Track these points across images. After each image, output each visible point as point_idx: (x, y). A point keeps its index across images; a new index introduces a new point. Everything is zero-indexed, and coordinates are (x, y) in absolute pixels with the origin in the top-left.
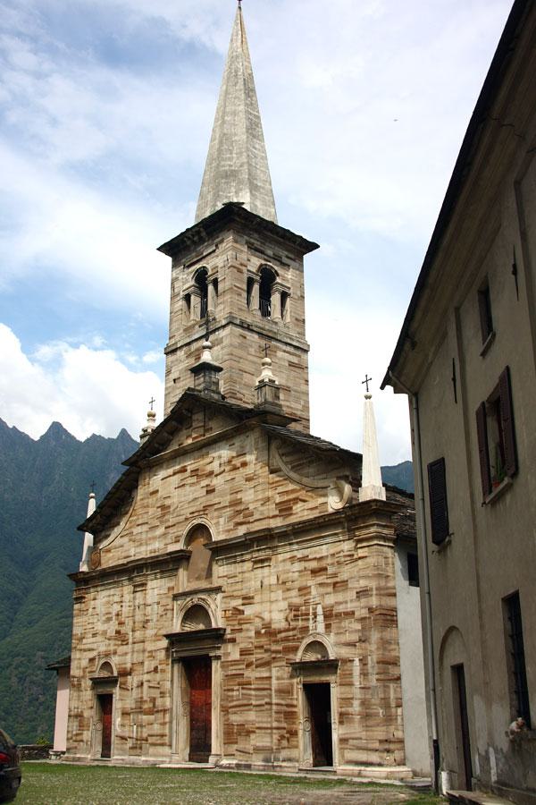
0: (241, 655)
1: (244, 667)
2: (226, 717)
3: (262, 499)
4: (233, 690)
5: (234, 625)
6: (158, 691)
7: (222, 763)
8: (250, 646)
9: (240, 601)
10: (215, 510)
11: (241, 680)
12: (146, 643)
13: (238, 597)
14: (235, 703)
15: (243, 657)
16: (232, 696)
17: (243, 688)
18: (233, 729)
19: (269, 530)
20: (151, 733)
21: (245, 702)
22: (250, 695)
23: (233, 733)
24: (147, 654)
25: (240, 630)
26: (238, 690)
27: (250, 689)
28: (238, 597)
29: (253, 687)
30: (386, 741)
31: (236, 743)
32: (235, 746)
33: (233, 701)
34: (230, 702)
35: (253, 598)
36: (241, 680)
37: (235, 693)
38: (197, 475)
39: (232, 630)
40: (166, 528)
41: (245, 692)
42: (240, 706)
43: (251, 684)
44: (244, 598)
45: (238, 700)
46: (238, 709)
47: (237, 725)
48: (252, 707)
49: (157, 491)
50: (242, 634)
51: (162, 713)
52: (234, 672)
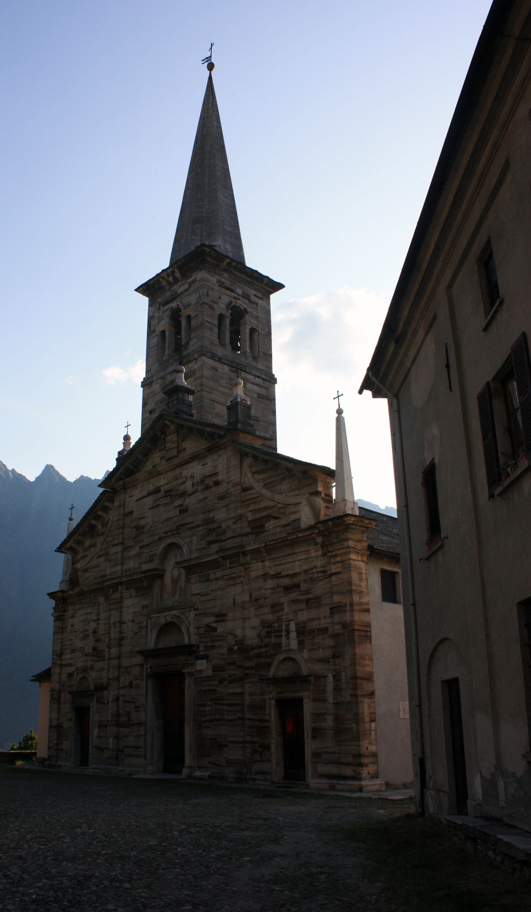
0: (213, 671)
1: (216, 683)
4: (205, 705)
9: (213, 619)
17: (216, 704)
27: (223, 704)
29: (225, 702)
37: (207, 708)
38: (171, 496)
39: (205, 647)
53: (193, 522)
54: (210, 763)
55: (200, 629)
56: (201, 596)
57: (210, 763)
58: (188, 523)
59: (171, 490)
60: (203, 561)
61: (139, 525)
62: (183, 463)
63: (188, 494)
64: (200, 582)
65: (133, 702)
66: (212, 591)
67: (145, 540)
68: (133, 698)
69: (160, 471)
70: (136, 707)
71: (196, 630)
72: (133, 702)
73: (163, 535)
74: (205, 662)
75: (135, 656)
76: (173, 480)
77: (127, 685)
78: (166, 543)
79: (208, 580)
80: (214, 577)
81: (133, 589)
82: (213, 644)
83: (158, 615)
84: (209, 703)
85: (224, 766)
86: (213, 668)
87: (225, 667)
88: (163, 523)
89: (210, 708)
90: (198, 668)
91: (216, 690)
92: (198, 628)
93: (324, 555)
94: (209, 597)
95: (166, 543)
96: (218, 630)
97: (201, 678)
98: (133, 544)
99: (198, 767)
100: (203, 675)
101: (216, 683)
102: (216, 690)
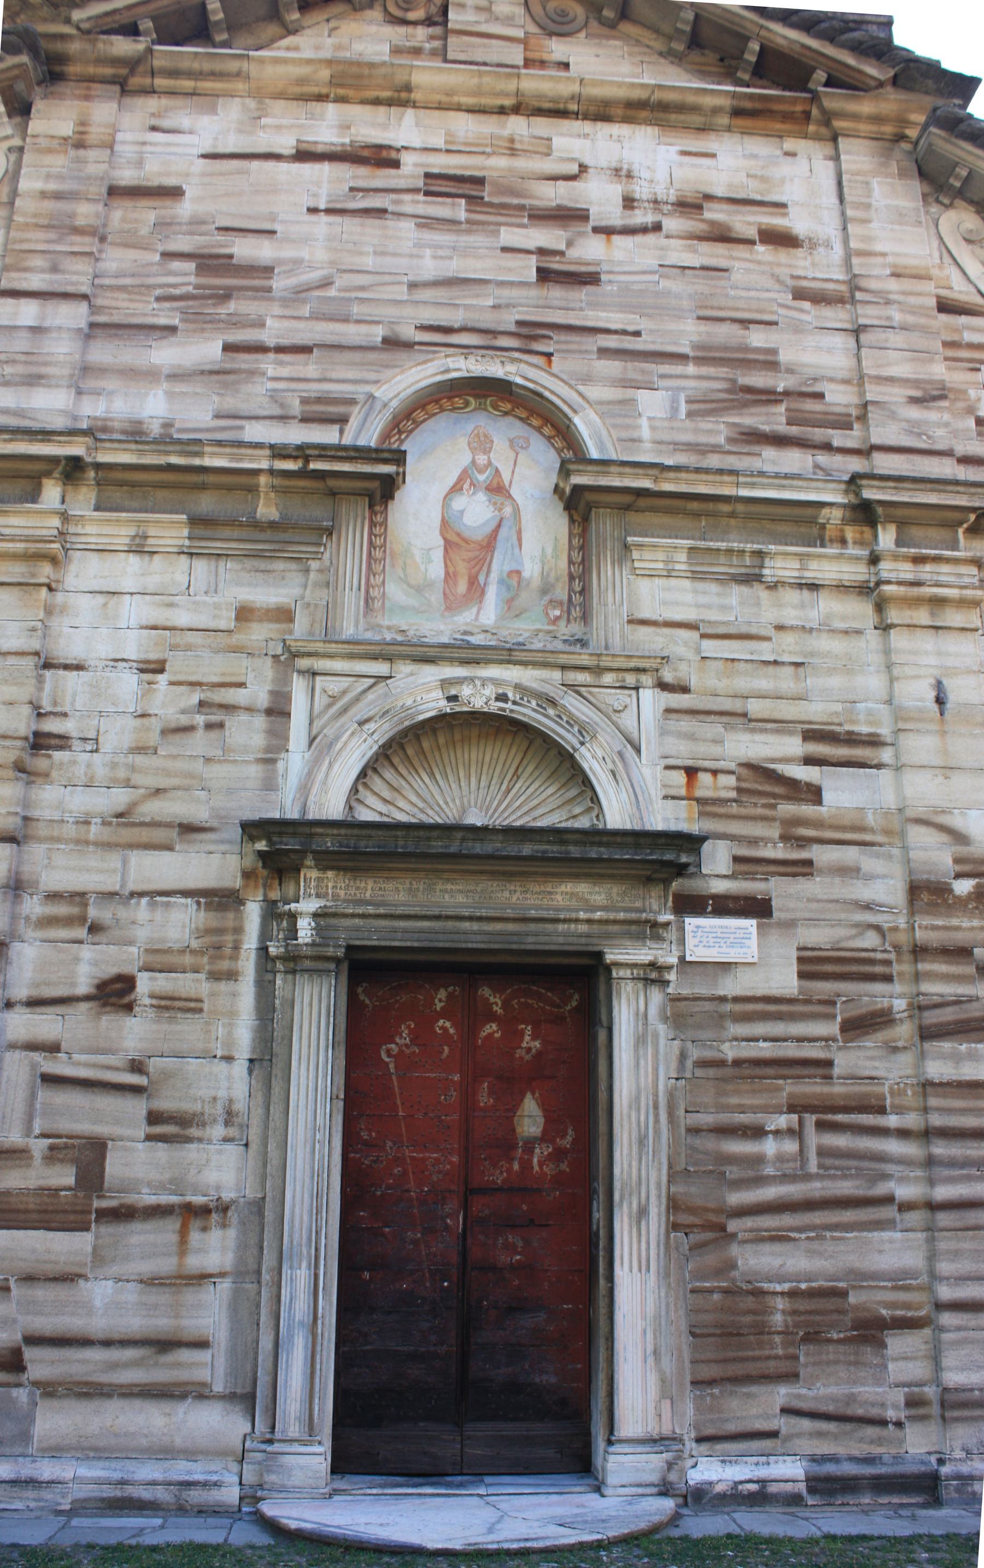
0: (802, 975)
1: (832, 1029)
2: (711, 1259)
3: (916, 383)
4: (758, 1132)
5: (754, 842)
6: (137, 1108)
7: (696, 1476)
8: (870, 940)
9: (794, 746)
10: (604, 352)
11: (812, 1088)
12: (37, 851)
13: (780, 725)
14: (769, 1193)
15: (825, 988)
16: (759, 1160)
17: (822, 1126)
18: (768, 1311)
19: (783, 122)
20: (45, 1324)
21: (846, 1188)
22: (881, 1158)
23: (761, 1330)
24: (33, 906)
25: (805, 868)
26: (796, 1133)
27: (883, 1132)
28: (780, 725)
29: (892, 1121)
30: (133, 486)
31: (791, 1377)
32: (782, 1394)
33: (760, 1181)
34: (738, 1184)
35: (874, 742)
36: (812, 1088)
37: (769, 1147)
38: (471, 199)
39: (737, 859)
40: (228, 348)
41: (840, 1141)
42: (809, 1205)
43: (882, 1110)
44: (810, 736)
45: (785, 1178)
46: (787, 1220)
47: (792, 1294)
48: (889, 1212)
49: (175, 193)
50: (803, 886)
51: (172, 1225)
52: (765, 1050)
53: (637, 334)
54: (786, 1411)
55: (704, 779)
56: (703, 636)
57: (786, 1411)
58: (607, 331)
59: (479, 181)
60: (744, 492)
61: (231, 257)
62: (574, 107)
63: (592, 223)
64: (696, 576)
65: (136, 1090)
66: (780, 628)
67: (269, 322)
68: (137, 1067)
69: (408, 88)
70: (154, 1118)
71: (680, 778)
72: (136, 1090)
73: (408, 332)
74: (754, 930)
75: (170, 848)
76: (488, 150)
77: (83, 987)
78: (448, 371)
79: (751, 578)
80: (796, 574)
81: (184, 517)
82: (804, 855)
83: (381, 668)
84: (782, 1121)
85: (899, 1424)
86: (801, 960)
87: (888, 963)
88: (413, 286)
89: (791, 1146)
90: (695, 953)
91: (829, 1063)
92: (691, 772)
93: (146, 537)
94: (765, 651)
95: (448, 371)
96: (827, 796)
97: (723, 999)
98: (176, 322)
99: (700, 1440)
100: (730, 986)
101: (832, 1029)
102: (829, 1063)
